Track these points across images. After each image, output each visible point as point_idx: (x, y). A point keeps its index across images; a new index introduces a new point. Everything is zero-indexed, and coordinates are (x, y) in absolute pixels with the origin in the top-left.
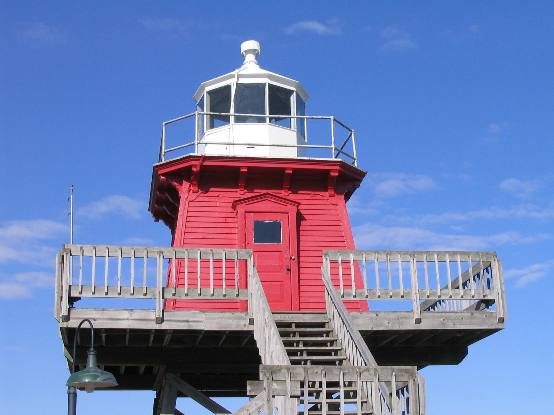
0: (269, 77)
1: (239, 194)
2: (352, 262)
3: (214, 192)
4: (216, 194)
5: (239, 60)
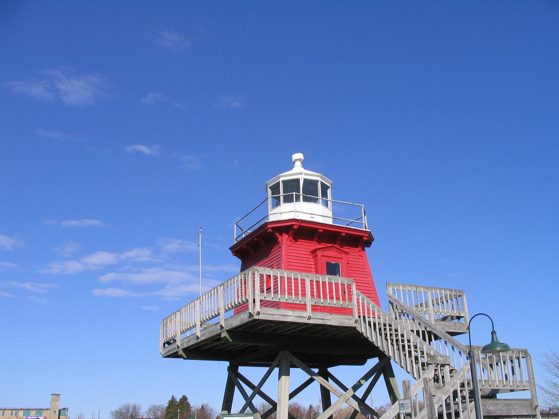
0: (321, 177)
1: (313, 245)
2: (286, 293)
3: (300, 242)
4: (301, 243)
5: (291, 166)
